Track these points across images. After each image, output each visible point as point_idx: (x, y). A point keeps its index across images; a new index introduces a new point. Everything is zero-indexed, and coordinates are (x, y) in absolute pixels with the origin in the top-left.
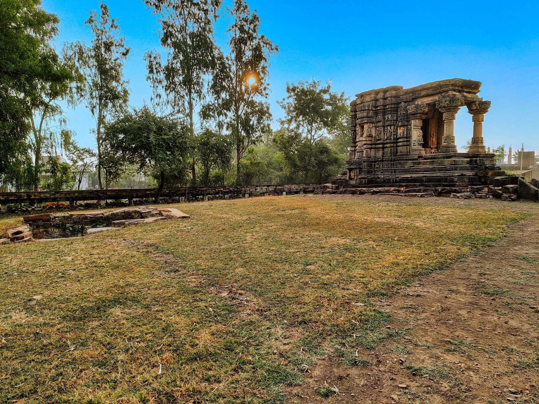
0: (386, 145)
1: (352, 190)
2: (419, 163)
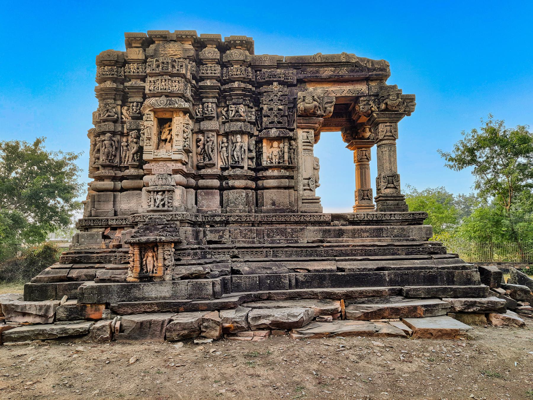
0: (231, 183)
1: (290, 294)
2: (340, 233)
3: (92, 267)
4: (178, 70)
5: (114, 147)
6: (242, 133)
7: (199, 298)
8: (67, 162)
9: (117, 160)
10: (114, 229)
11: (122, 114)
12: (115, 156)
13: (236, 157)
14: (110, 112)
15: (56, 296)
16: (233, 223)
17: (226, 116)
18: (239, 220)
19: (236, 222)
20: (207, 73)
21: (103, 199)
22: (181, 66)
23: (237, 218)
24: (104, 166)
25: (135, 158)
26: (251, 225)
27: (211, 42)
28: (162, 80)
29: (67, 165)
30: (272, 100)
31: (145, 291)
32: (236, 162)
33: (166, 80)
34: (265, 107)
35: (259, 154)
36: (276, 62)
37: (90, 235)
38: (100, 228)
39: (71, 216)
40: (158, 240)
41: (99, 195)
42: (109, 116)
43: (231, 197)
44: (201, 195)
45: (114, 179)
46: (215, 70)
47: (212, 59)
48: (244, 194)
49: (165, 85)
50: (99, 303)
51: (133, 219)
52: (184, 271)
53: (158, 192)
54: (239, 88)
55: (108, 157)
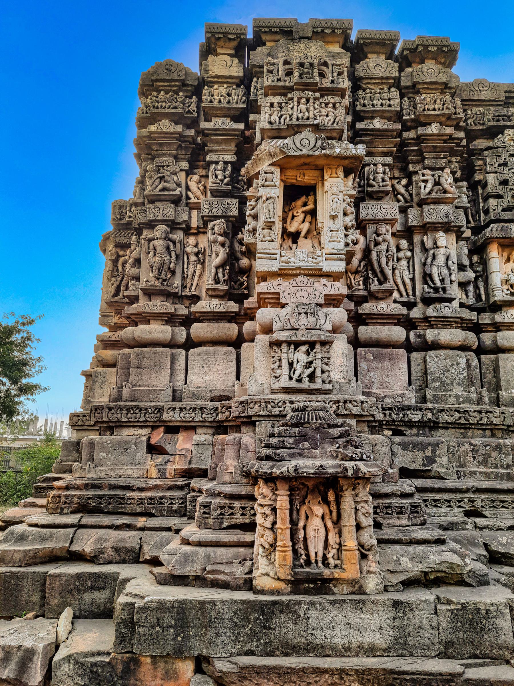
3: (129, 527)
4: (332, 82)
5: (173, 254)
6: (447, 227)
7: (476, 657)
8: (20, 327)
9: (177, 281)
10: (172, 430)
11: (188, 188)
12: (173, 272)
13: (436, 278)
14: (167, 182)
15: (42, 606)
16: (447, 428)
17: (407, 195)
18: (463, 421)
19: (456, 425)
20: (373, 105)
21: (147, 362)
22: (340, 74)
23: (457, 415)
24: (149, 294)
25: (220, 275)
26: (488, 433)
27: (377, 49)
28: (299, 99)
29: (18, 331)
30: (505, 164)
31: (312, 624)
32: (436, 290)
33: (308, 101)
34: (491, 178)
35: (484, 275)
36: (504, 94)
37: (120, 442)
38: (141, 427)
39: (18, 403)
40: (350, 472)
41: (139, 354)
42: (164, 189)
43: (432, 366)
44: (366, 360)
45: (170, 319)
46: (389, 100)
47: (382, 78)
48: (463, 362)
49: (308, 110)
50: (179, 653)
51: (241, 408)
52: (408, 562)
53: (297, 345)
54: (438, 136)
55: (160, 273)
